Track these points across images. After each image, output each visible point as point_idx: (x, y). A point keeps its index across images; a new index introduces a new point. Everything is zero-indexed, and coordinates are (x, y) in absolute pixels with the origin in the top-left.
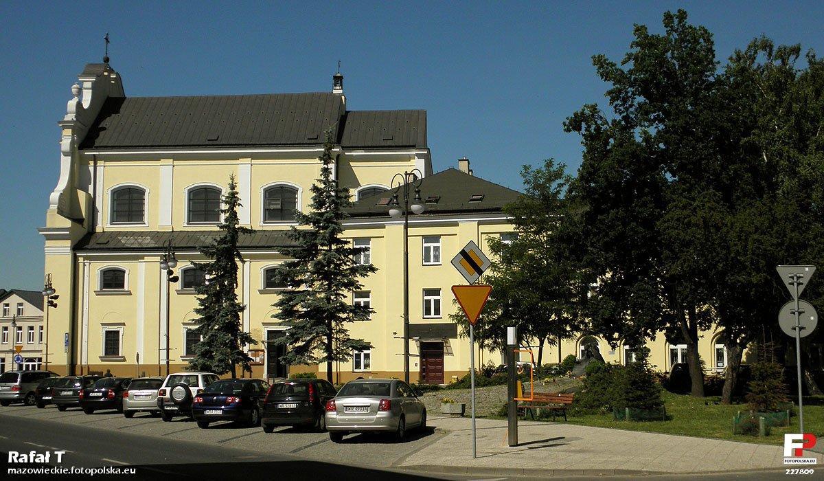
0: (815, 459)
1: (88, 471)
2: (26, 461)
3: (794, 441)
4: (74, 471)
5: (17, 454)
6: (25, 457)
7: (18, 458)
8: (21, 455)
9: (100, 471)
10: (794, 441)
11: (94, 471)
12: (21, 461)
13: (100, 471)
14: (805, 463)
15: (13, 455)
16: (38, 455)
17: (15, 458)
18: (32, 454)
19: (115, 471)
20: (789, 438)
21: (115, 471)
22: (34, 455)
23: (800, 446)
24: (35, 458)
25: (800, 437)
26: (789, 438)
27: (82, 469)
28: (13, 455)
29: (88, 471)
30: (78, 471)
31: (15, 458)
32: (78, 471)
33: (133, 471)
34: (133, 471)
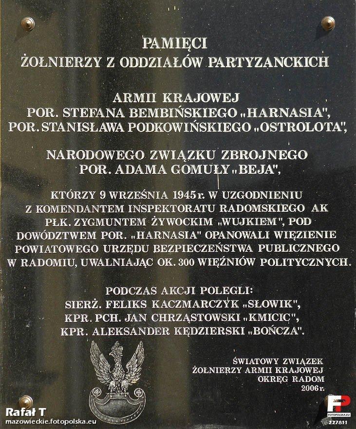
0: (350, 413)
1: (62, 422)
2: (18, 415)
4: (52, 422)
5: (12, 410)
6: (18, 412)
7: (13, 413)
8: (15, 411)
9: (71, 422)
11: (67, 422)
12: (15, 414)
13: (71, 422)
15: (10, 410)
17: (10, 413)
18: (23, 410)
19: (81, 422)
21: (81, 422)
22: (24, 411)
23: (339, 404)
24: (25, 412)
25: (339, 397)
27: (58, 420)
28: (10, 410)
29: (62, 422)
30: (55, 422)
31: (10, 413)
32: (55, 422)
33: (94, 422)
34: (94, 422)
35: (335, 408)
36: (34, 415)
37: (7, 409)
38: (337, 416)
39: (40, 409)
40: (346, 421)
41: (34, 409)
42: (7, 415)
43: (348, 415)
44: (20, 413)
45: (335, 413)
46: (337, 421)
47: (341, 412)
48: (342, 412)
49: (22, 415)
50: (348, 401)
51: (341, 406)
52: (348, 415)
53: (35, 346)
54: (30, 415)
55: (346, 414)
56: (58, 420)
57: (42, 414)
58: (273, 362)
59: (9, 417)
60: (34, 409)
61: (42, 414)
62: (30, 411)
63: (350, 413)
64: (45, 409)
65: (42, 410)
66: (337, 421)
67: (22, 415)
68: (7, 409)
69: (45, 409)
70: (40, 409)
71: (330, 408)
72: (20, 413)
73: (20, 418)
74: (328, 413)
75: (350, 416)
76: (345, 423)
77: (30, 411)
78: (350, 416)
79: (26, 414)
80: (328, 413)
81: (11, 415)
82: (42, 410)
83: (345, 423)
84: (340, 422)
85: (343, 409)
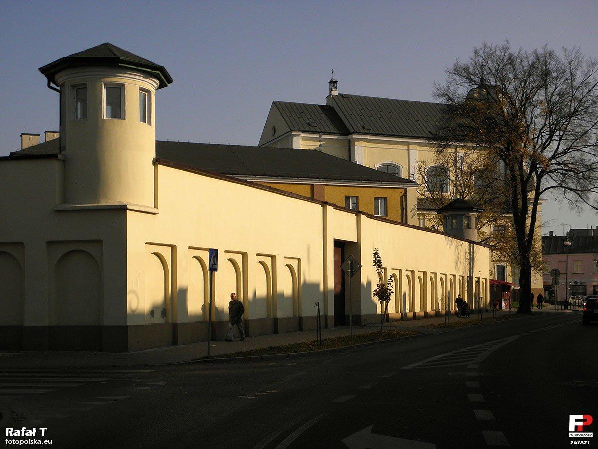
0: (592, 433)
1: (17, 442)
2: (19, 435)
3: (576, 420)
4: (8, 441)
5: (12, 429)
6: (18, 431)
7: (13, 432)
8: (15, 430)
9: (26, 442)
10: (576, 420)
11: (22, 442)
12: (15, 434)
13: (26, 442)
14: (584, 436)
15: (10, 430)
16: (27, 430)
17: (11, 432)
18: (23, 429)
19: (37, 442)
20: (572, 418)
21: (37, 442)
22: (25, 430)
23: (580, 423)
24: (25, 432)
25: (581, 417)
26: (572, 418)
27: (14, 440)
28: (10, 430)
29: (17, 442)
30: (10, 442)
31: (11, 432)
32: (10, 442)
33: (50, 442)
34: (50, 442)
35: (576, 427)
36: (34, 435)
37: (8, 429)
38: (578, 436)
39: (41, 428)
40: (588, 441)
41: (34, 429)
42: (7, 434)
43: (590, 434)
44: (21, 432)
45: (577, 433)
46: (579, 441)
47: (583, 432)
48: (586, 432)
49: (23, 434)
50: (590, 419)
51: (583, 426)
52: (590, 434)
53: (490, 56)
54: (31, 435)
55: (587, 433)
56: (14, 440)
57: (43, 434)
58: (540, 306)
59: (10, 437)
60: (34, 429)
61: (43, 434)
62: (30, 431)
63: (592, 433)
64: (46, 428)
65: (43, 429)
66: (579, 441)
67: (23, 434)
68: (8, 429)
69: (46, 428)
70: (41, 428)
71: (571, 428)
72: (21, 432)
73: (20, 438)
74: (569, 433)
75: (592, 436)
76: (587, 443)
77: (30, 431)
78: (592, 436)
79: (27, 434)
80: (569, 433)
81: (11, 435)
82: (43, 429)
83: (587, 443)
84: (582, 441)
85: (585, 429)
